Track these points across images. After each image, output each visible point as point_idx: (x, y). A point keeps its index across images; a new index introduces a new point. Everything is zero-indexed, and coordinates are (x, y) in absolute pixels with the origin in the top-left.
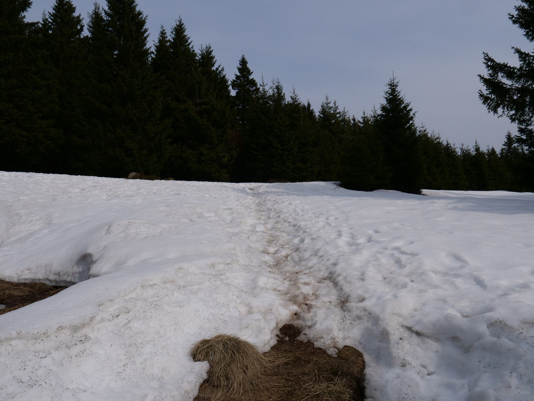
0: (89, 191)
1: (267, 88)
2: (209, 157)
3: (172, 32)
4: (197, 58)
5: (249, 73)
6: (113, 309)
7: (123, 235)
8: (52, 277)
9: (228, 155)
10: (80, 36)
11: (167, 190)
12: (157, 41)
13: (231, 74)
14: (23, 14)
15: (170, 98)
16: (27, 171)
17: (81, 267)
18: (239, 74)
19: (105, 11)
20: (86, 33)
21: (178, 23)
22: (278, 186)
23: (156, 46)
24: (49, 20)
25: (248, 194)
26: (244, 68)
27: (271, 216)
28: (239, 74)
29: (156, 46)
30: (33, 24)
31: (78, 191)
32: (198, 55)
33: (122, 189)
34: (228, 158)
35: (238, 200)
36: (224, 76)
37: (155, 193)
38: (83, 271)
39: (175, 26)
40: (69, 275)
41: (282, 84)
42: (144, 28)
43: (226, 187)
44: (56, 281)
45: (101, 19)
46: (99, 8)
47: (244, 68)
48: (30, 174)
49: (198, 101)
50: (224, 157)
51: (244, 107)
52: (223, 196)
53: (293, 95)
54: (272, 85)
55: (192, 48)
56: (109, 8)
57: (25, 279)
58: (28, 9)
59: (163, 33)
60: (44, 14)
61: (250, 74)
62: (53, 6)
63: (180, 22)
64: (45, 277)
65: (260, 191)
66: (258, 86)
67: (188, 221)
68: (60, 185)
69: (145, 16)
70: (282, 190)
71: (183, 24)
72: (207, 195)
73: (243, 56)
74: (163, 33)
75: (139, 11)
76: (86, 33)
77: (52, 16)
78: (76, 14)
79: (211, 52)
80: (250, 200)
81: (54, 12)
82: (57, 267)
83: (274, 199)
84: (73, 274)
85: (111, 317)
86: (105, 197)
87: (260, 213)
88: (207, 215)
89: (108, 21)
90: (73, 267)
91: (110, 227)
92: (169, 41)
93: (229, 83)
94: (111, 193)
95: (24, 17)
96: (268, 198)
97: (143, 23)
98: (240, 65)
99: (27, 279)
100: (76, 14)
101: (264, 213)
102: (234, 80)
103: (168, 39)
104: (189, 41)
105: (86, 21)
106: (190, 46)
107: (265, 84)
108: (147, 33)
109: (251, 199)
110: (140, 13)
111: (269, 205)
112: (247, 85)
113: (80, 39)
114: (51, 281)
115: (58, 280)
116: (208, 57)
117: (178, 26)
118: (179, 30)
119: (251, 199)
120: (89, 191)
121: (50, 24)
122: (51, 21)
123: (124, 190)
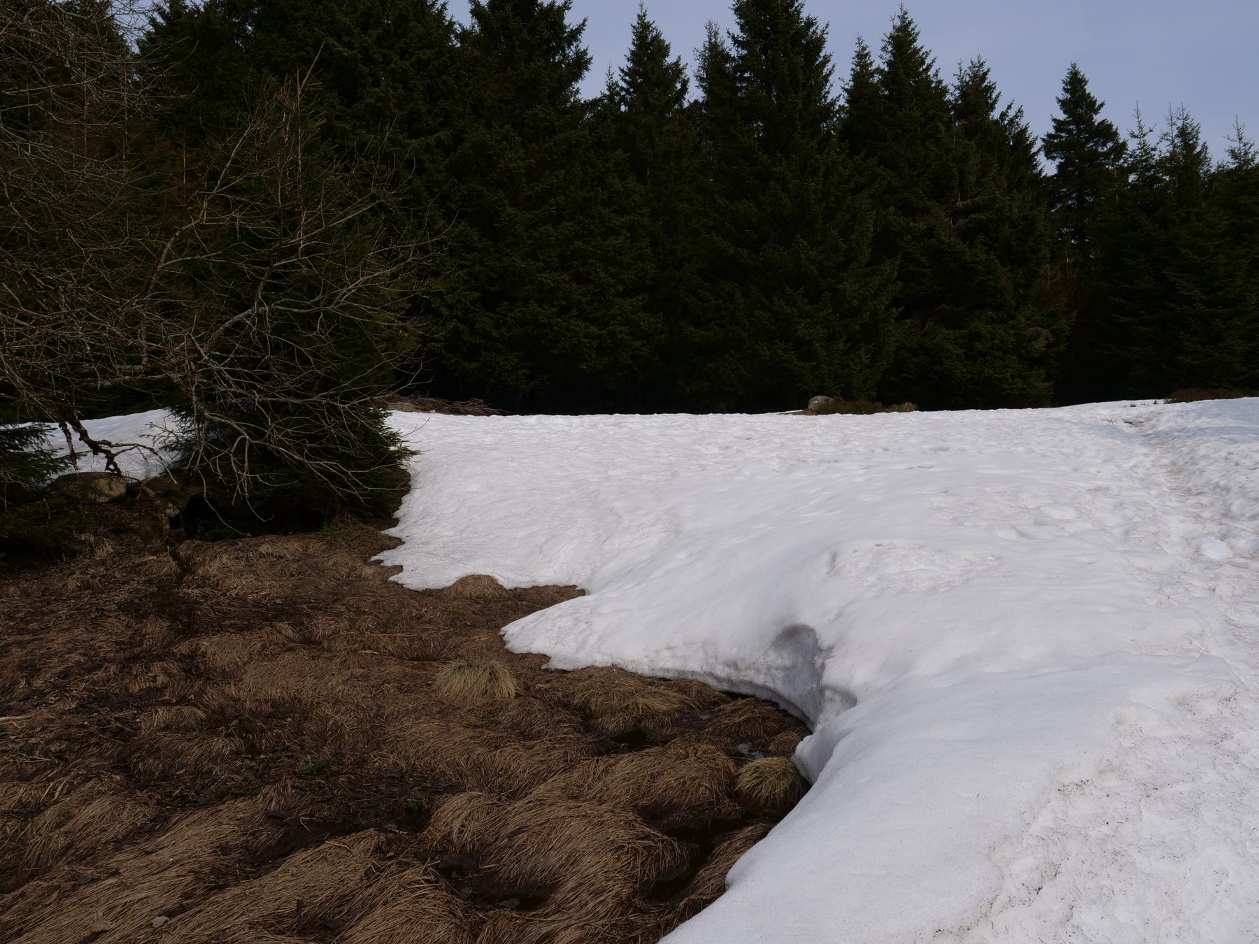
0: (738, 451)
1: (1151, 140)
2: (996, 341)
3: (884, 49)
4: (948, 97)
5: (1093, 106)
6: (1023, 867)
7: (872, 579)
8: (721, 671)
9: (1045, 332)
10: (681, 105)
11: (914, 440)
12: (848, 76)
13: (1040, 117)
14: (576, 85)
15: (892, 209)
16: (611, 412)
17: (785, 654)
18: (1062, 116)
19: (733, 37)
20: (695, 93)
21: (898, 23)
22: (1215, 410)
23: (846, 90)
24: (622, 84)
25: (1129, 437)
26: (1077, 98)
27: (1234, 508)
28: (1062, 116)
29: (846, 90)
30: (595, 103)
31: (716, 451)
32: (951, 89)
33: (807, 442)
34: (1047, 339)
35: (1107, 461)
36: (1024, 131)
37: (886, 450)
38: (794, 667)
39: (890, 30)
40: (758, 671)
41: (1196, 119)
42: (822, 54)
43: (1060, 420)
44: (730, 681)
45: (727, 58)
46: (716, 33)
47: (1077, 98)
48: (617, 417)
49: (959, 204)
50: (1035, 337)
51: (1081, 201)
52: (1065, 450)
53: (1236, 145)
54: (1166, 129)
55: (936, 75)
56: (742, 29)
57: (663, 669)
58: (586, 73)
59: (862, 56)
60: (610, 75)
61: (1096, 111)
62: (629, 54)
63: (903, 18)
64: (706, 668)
65: (1162, 427)
66: (1123, 136)
67: (1013, 535)
68: (678, 439)
69: (821, 27)
70: (1232, 423)
71: (910, 23)
72: (1021, 449)
73: (1074, 66)
74: (862, 56)
75: (808, 19)
76: (695, 93)
77: (626, 74)
78: (670, 60)
79: (985, 74)
80: (1143, 457)
81: (630, 65)
82: (729, 650)
83: (1223, 454)
84: (769, 668)
85: (1024, 894)
86: (775, 464)
87: (1192, 500)
88: (1056, 514)
89: (742, 57)
90: (766, 654)
91: (834, 557)
92: (878, 70)
93: (1039, 144)
94: (786, 454)
95: (577, 92)
96: (1202, 451)
97: (819, 43)
98: (1066, 90)
99: (668, 670)
100: (670, 60)
101: (1204, 500)
102: (1050, 136)
103: (874, 67)
104: (928, 61)
105: (692, 69)
106: (931, 73)
107: (1146, 130)
108: (829, 66)
109: (1146, 455)
110: (810, 23)
111: (1214, 473)
112: (1088, 140)
113: (682, 111)
114: (718, 679)
115: (734, 678)
116: (977, 91)
117: (898, 30)
118: (902, 40)
119: (1146, 455)
120: (738, 451)
121: (623, 93)
122: (625, 86)
123: (813, 444)
